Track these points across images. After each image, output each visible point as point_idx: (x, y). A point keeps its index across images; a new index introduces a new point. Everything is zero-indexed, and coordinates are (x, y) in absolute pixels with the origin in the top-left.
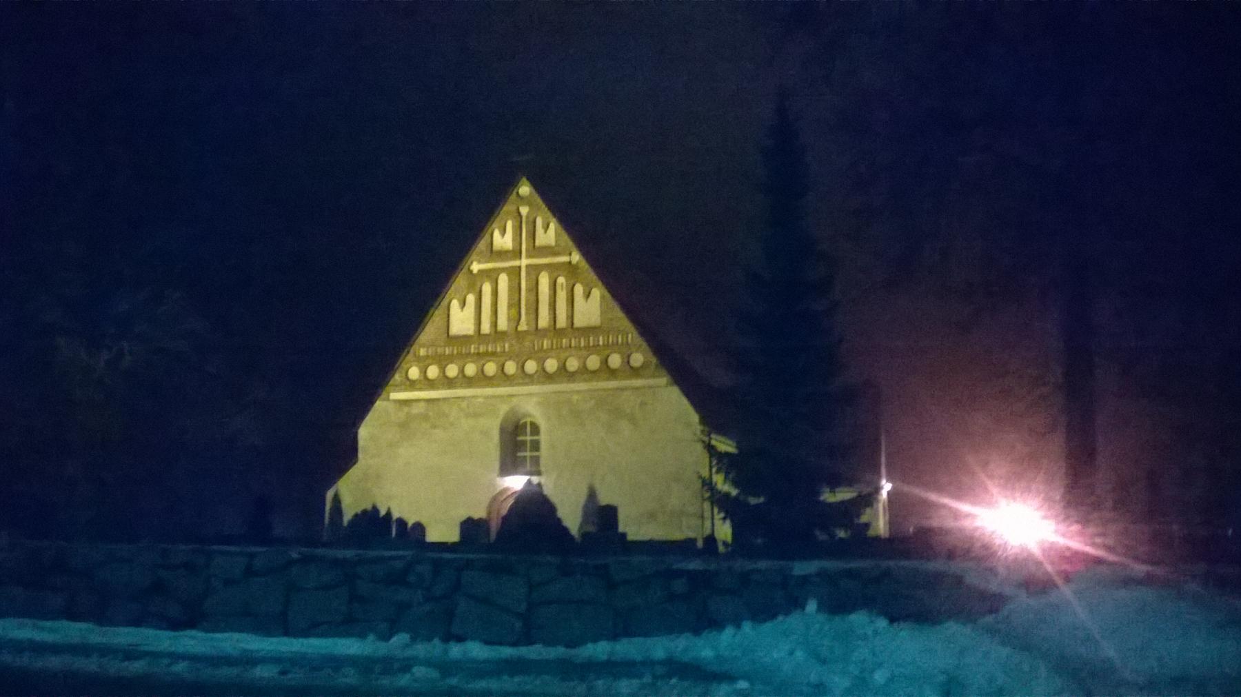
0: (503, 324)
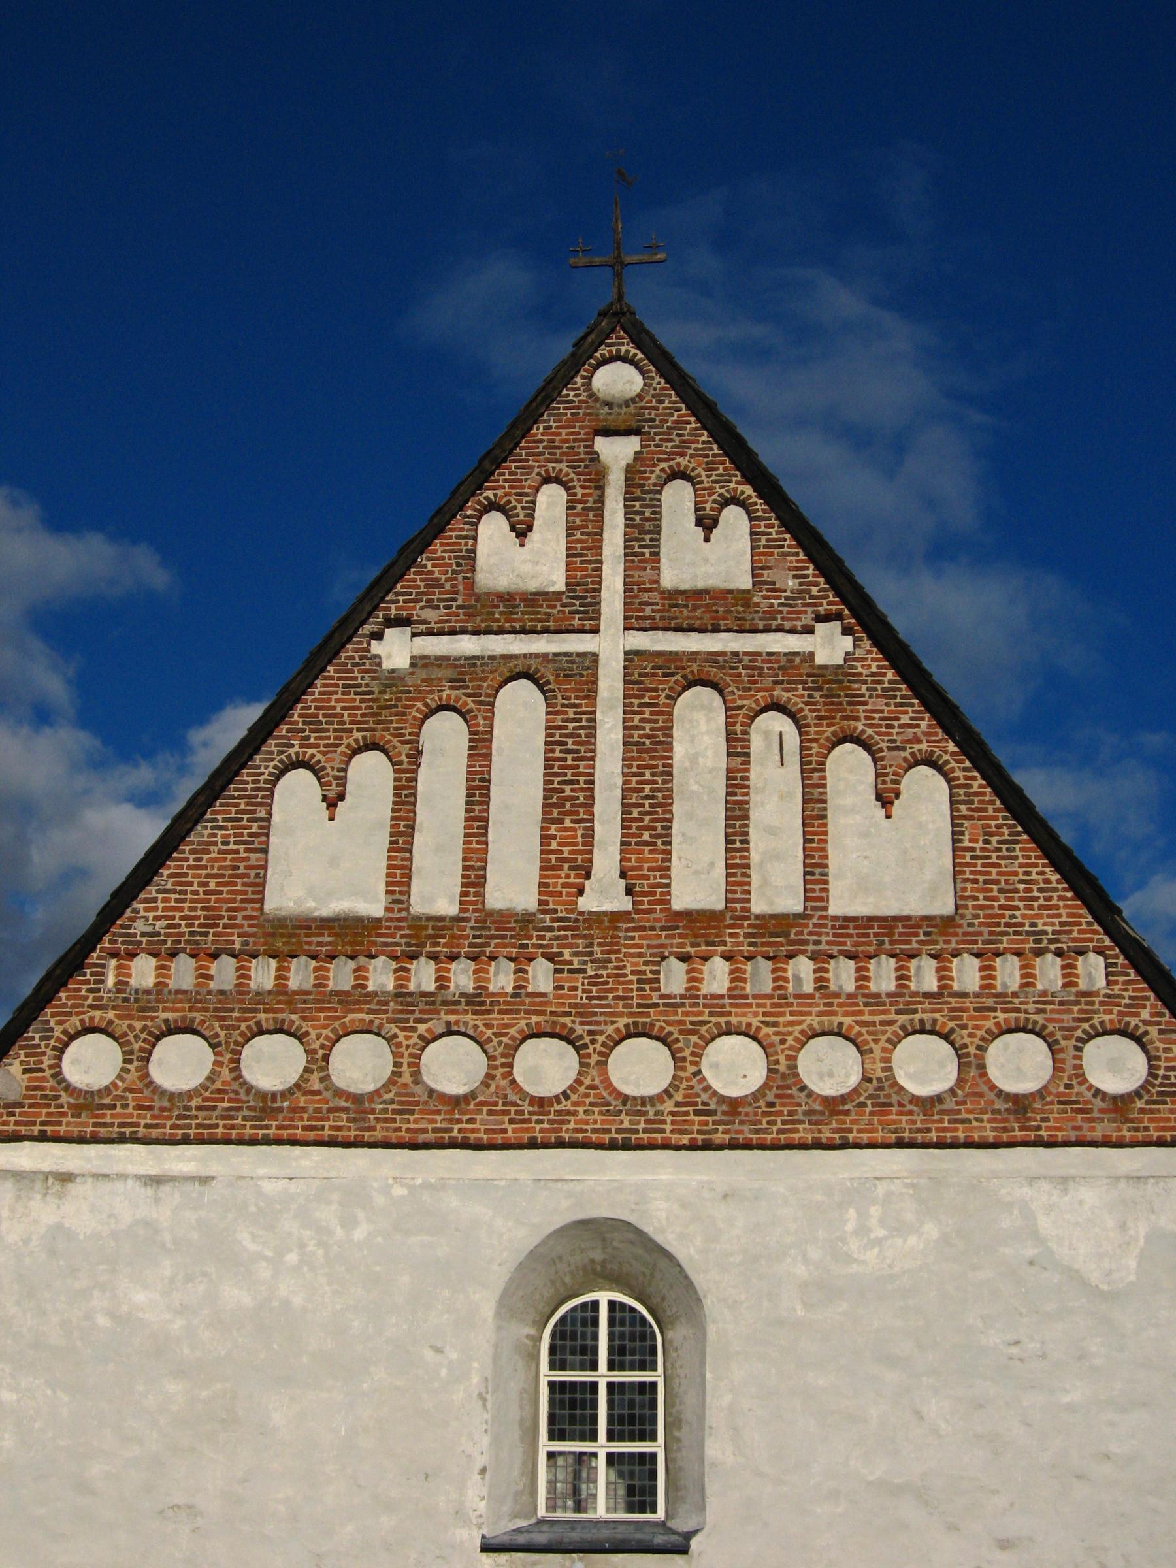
0: (513, 886)
